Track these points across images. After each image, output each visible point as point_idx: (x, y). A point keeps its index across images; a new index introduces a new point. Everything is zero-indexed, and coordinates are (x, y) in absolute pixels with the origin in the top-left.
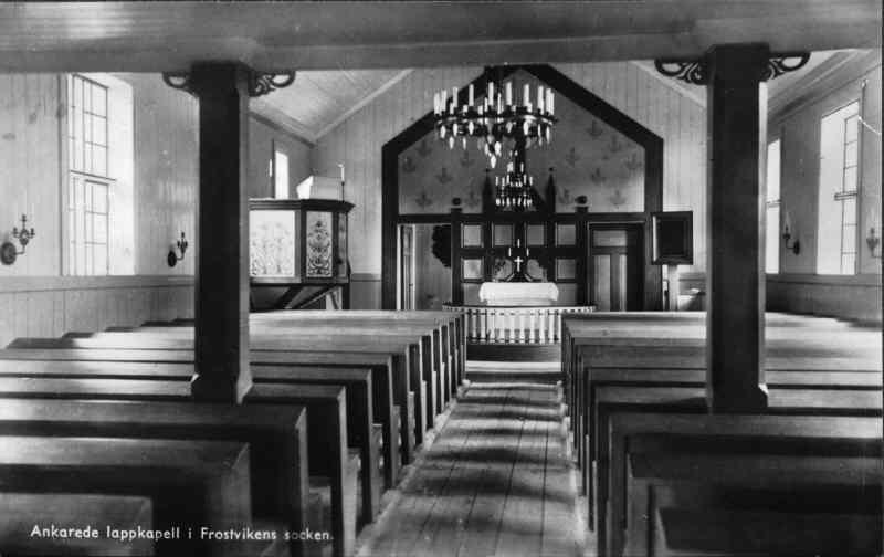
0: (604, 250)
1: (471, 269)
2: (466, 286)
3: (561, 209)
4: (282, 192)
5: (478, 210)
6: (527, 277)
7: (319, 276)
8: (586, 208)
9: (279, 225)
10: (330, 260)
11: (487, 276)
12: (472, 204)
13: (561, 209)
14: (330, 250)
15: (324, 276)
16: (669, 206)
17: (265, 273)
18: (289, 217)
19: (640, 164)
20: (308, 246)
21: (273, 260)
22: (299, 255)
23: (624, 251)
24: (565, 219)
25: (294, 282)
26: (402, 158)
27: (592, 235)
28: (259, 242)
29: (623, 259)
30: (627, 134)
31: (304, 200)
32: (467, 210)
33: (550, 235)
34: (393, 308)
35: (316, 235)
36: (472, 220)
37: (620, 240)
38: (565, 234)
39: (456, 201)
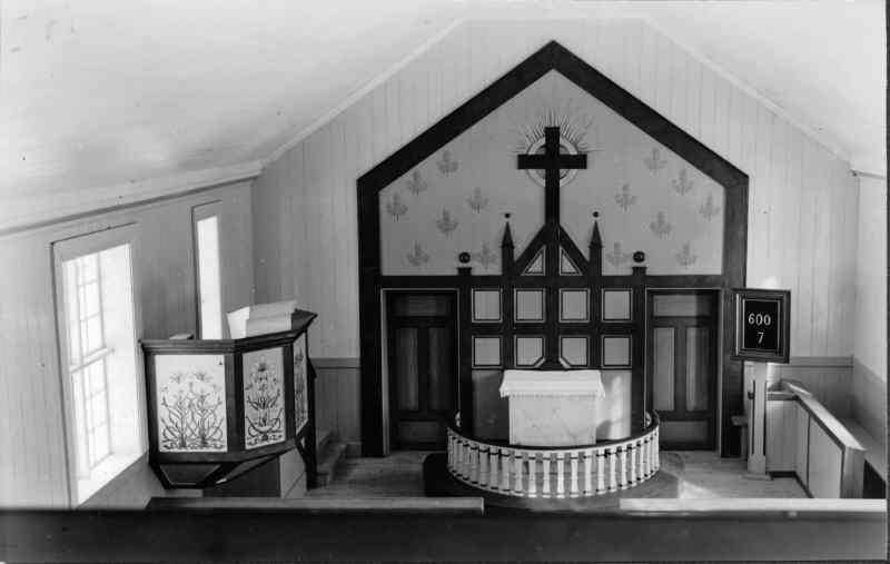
0: (665, 321)
1: (487, 351)
2: (477, 376)
3: (609, 269)
4: (211, 330)
5: (495, 269)
6: (562, 362)
7: (265, 443)
8: (644, 269)
9: (202, 377)
10: (282, 417)
11: (508, 360)
12: (485, 260)
13: (609, 269)
14: (281, 402)
15: (272, 442)
16: (762, 276)
17: (183, 445)
18: (215, 366)
19: (718, 210)
20: (247, 405)
21: (193, 426)
22: (232, 392)
23: (694, 322)
24: (616, 283)
25: (227, 459)
26: (387, 195)
27: (651, 303)
28: (171, 402)
29: (692, 333)
30: (685, 155)
31: (236, 341)
32: (479, 269)
33: (596, 304)
34: (379, 454)
35: (258, 385)
36: (487, 283)
37: (688, 307)
38: (617, 305)
39: (464, 257)
